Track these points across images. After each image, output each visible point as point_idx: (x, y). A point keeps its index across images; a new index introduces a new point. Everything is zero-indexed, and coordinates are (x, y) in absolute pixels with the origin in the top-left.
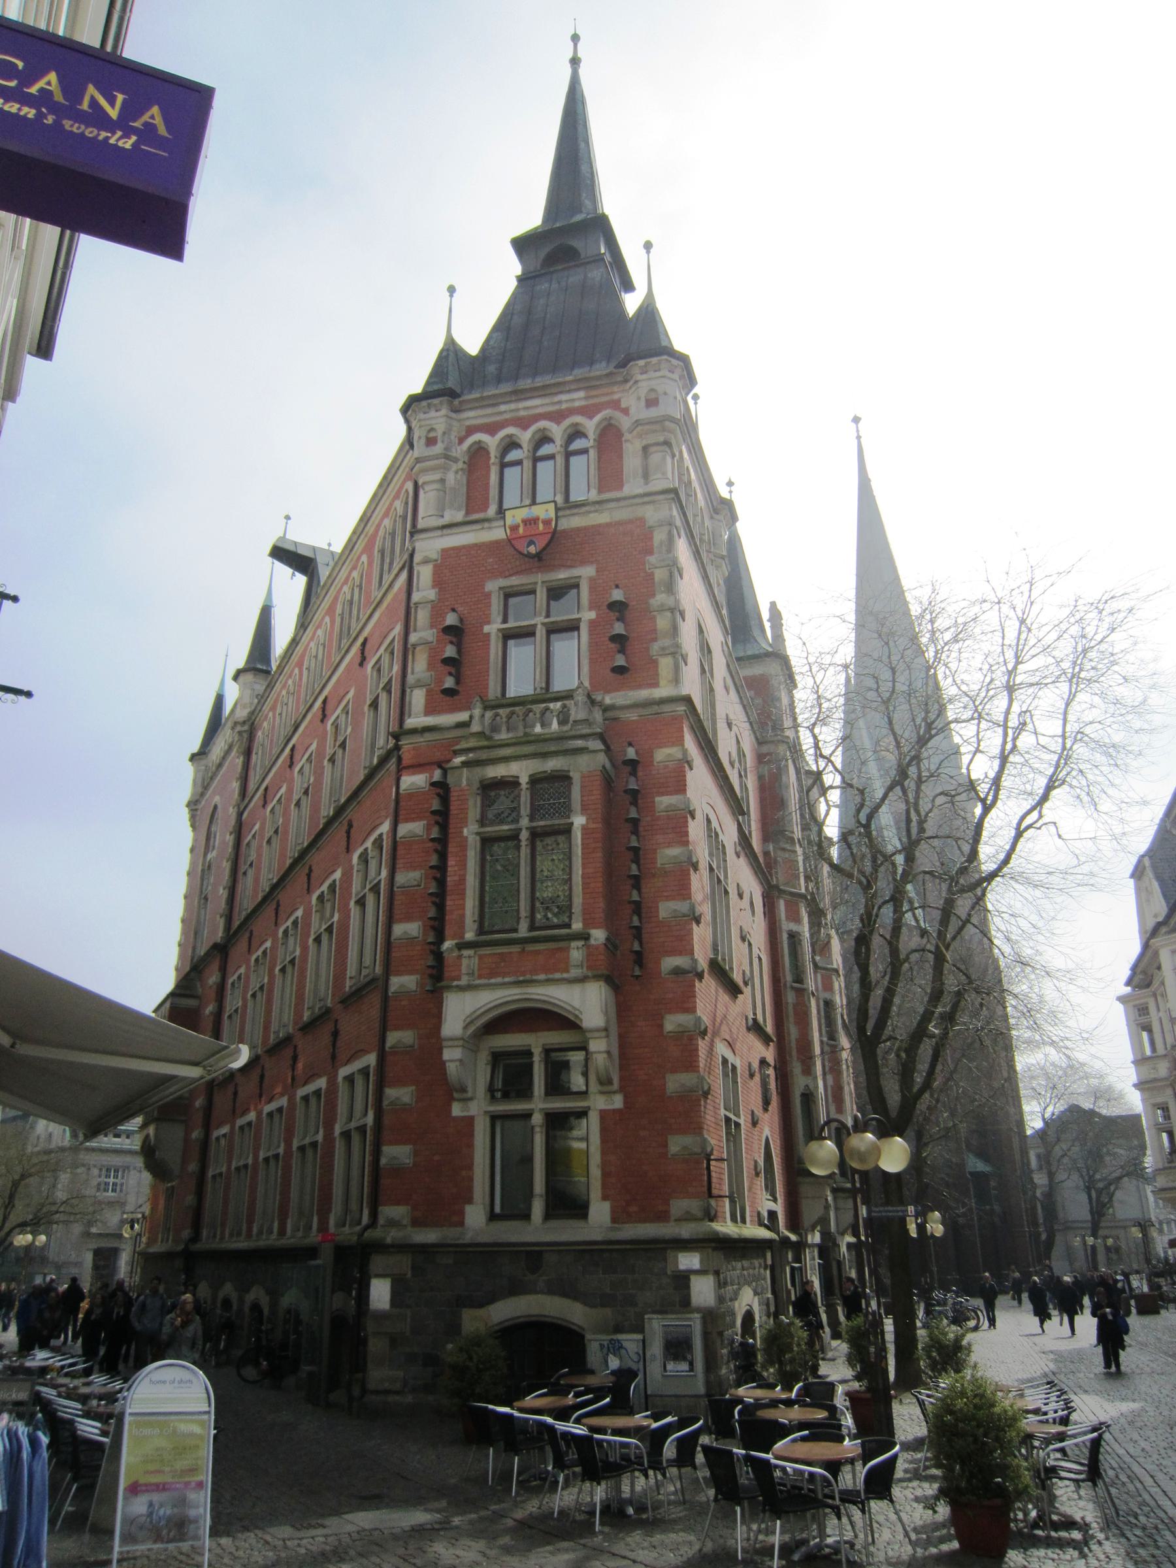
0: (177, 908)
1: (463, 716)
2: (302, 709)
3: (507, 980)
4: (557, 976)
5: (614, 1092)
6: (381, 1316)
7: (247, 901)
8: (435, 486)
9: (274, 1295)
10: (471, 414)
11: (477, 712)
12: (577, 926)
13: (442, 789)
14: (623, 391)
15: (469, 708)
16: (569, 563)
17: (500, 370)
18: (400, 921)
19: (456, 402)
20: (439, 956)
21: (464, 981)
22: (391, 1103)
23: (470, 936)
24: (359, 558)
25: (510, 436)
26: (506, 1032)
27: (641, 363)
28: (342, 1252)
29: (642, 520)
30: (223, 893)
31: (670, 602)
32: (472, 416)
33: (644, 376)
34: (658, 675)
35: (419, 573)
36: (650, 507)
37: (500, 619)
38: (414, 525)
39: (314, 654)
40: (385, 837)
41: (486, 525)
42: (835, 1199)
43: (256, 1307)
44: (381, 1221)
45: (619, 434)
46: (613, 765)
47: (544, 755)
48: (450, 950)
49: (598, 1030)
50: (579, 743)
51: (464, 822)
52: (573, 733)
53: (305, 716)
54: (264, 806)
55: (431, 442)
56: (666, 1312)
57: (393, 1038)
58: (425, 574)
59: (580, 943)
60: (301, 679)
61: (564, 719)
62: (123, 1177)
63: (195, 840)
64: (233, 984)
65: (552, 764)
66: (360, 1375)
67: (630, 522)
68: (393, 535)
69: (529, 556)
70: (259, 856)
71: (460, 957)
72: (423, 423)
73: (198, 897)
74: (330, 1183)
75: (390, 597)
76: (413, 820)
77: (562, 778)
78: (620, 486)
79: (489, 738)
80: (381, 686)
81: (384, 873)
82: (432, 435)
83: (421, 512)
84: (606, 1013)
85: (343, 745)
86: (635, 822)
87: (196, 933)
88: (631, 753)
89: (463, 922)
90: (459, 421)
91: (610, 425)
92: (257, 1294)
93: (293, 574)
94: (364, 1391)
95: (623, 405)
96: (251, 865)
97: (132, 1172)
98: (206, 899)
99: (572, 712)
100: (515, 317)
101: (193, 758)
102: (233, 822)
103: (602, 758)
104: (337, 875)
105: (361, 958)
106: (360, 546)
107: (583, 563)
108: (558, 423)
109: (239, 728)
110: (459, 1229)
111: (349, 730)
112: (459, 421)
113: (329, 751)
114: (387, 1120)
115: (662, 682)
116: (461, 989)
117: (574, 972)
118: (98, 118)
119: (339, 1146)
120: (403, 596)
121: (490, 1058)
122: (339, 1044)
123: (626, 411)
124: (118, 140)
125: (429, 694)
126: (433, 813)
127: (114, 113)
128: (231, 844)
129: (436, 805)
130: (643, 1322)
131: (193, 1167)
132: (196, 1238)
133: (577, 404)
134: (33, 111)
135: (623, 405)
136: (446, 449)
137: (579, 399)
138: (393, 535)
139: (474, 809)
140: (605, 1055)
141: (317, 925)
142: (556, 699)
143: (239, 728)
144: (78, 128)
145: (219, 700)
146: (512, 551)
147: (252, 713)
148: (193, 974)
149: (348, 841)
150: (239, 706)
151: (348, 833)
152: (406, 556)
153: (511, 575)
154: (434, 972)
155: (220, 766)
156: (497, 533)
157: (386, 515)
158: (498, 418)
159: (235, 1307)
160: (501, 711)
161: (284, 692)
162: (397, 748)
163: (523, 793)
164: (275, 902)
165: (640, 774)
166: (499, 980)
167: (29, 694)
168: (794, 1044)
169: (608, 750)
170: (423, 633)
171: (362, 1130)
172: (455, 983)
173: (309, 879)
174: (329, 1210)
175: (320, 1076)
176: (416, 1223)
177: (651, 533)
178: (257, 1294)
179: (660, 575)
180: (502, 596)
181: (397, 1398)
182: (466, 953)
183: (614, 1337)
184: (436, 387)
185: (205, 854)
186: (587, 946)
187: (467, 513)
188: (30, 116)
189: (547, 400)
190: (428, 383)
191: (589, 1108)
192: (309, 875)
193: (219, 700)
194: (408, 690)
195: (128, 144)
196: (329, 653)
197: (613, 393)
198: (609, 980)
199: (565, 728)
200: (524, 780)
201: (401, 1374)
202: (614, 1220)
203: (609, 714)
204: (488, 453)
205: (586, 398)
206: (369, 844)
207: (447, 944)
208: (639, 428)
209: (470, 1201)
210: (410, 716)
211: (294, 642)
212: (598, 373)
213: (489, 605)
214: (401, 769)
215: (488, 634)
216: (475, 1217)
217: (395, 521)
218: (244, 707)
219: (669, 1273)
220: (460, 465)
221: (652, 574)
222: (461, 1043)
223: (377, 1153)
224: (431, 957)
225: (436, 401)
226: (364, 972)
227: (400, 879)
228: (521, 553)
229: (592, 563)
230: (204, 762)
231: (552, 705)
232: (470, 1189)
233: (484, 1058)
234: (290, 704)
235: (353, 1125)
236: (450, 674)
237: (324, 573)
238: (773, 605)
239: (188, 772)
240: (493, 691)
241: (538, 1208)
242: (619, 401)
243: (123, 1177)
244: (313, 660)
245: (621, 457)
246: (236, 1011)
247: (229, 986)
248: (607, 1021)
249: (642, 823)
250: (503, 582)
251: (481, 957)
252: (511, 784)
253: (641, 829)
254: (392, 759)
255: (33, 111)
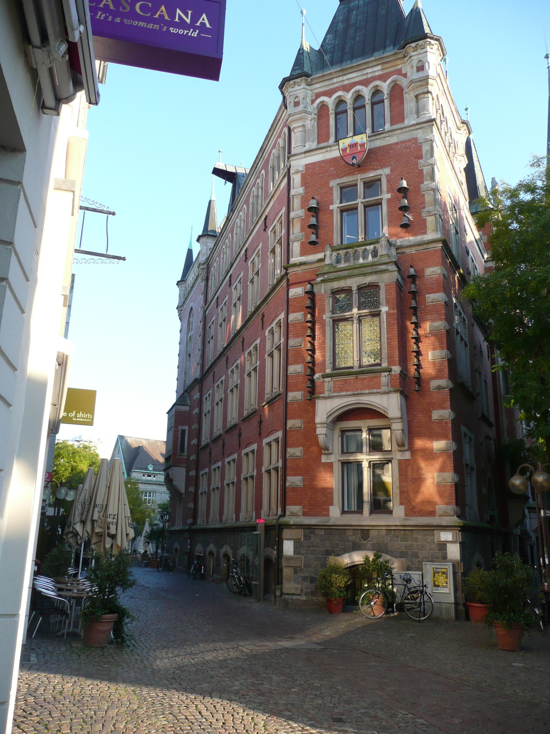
0: (175, 361)
1: (320, 256)
2: (234, 255)
3: (348, 393)
4: (375, 391)
5: (406, 451)
6: (289, 558)
7: (210, 358)
8: (300, 129)
9: (235, 550)
10: (318, 85)
11: (328, 253)
12: (385, 365)
13: (311, 294)
14: (403, 63)
15: (323, 251)
16: (375, 167)
17: (332, 57)
18: (292, 364)
19: (309, 79)
20: (312, 381)
21: (326, 394)
22: (291, 456)
23: (328, 371)
24: (260, 171)
25: (340, 97)
26: (349, 420)
27: (413, 45)
28: (268, 528)
29: (416, 139)
30: (198, 353)
31: (433, 185)
32: (319, 87)
33: (415, 53)
34: (426, 227)
35: (293, 179)
36: (420, 131)
37: (338, 201)
38: (289, 152)
39: (239, 225)
40: (282, 321)
41: (329, 149)
42: (529, 512)
43: (226, 556)
44: (288, 513)
45: (402, 89)
46: (402, 278)
47: (365, 274)
48: (319, 378)
49: (397, 419)
50: (383, 267)
51: (323, 311)
52: (380, 262)
53: (236, 259)
54: (217, 307)
55: (297, 104)
56: (434, 562)
57: (290, 423)
58: (297, 179)
59: (387, 374)
60: (233, 239)
61: (375, 253)
62: (153, 496)
63: (182, 326)
64: (206, 398)
65: (369, 279)
66: (280, 586)
67: (409, 141)
68: (278, 158)
69: (353, 165)
70: (216, 333)
71: (323, 382)
72: (291, 94)
73: (185, 355)
74: (261, 495)
75: (278, 193)
76: (297, 312)
77: (375, 286)
78: (402, 120)
79: (334, 267)
80: (276, 241)
81: (282, 340)
82: (297, 100)
83: (293, 145)
84: (401, 410)
85: (257, 274)
86: (415, 309)
87: (185, 373)
88: (412, 271)
89: (325, 364)
90: (311, 90)
91: (396, 84)
92: (226, 549)
93: (226, 183)
94: (282, 594)
95: (403, 72)
96: (212, 338)
97: (158, 494)
98: (189, 355)
99: (379, 251)
100: (340, 24)
101: (178, 283)
102: (201, 316)
103: (396, 275)
104: (258, 341)
105: (272, 385)
106: (260, 165)
107: (383, 167)
108: (366, 86)
109: (201, 267)
110: (326, 518)
111: (260, 266)
112: (311, 90)
113: (250, 277)
114: (288, 464)
115: (428, 232)
116: (325, 398)
117: (384, 389)
118: (182, 24)
119: (265, 477)
120: (286, 191)
121: (340, 433)
122: (262, 426)
123: (405, 75)
124: (191, 33)
125: (302, 244)
126: (307, 307)
127: (188, 21)
128: (201, 327)
129: (308, 303)
130: (422, 566)
131: (192, 489)
132: (195, 522)
133: (377, 74)
134: (158, 26)
135: (403, 72)
136: (305, 107)
137: (378, 71)
138: (278, 158)
139: (328, 303)
140: (401, 431)
141: (248, 368)
142: (370, 244)
143: (201, 267)
144: (176, 31)
145: (190, 252)
146: (344, 163)
147: (208, 259)
148: (186, 394)
149: (263, 324)
150: (200, 255)
151: (262, 320)
152: (286, 170)
153: (343, 177)
154: (310, 390)
155: (192, 287)
156: (335, 153)
157: (274, 147)
158: (332, 87)
159: (215, 556)
160: (340, 252)
161: (224, 247)
162: (286, 274)
163: (354, 295)
164: (226, 356)
165: (417, 282)
166: (344, 393)
167: (124, 259)
168: (505, 428)
169: (399, 270)
170: (298, 212)
171: (276, 469)
172: (322, 395)
173: (243, 344)
174: (261, 508)
175: (254, 443)
176: (305, 514)
177: (421, 146)
178: (226, 549)
179: (426, 170)
180: (339, 188)
181: (298, 597)
182: (326, 379)
183: (407, 572)
184: (297, 72)
185: (188, 333)
186: (391, 375)
187: (319, 143)
188: (158, 29)
189: (359, 73)
190: (293, 70)
191: (392, 458)
192: (243, 342)
193: (190, 252)
194: (291, 243)
195: (195, 34)
196: (247, 224)
197: (397, 65)
198: (402, 393)
199: (376, 259)
200: (354, 288)
201: (300, 586)
202: (406, 515)
203: (399, 251)
204: (328, 108)
205: (382, 69)
206: (274, 325)
207: (316, 376)
208: (413, 85)
209: (332, 504)
210: (292, 257)
211: (228, 219)
212: (388, 54)
213: (332, 194)
214: (289, 286)
215: (332, 210)
216: (335, 512)
217: (279, 150)
218: (203, 255)
219: (436, 542)
220: (313, 116)
221: (422, 170)
222: (325, 425)
223: (284, 480)
224: (309, 382)
225: (298, 80)
226: (274, 391)
227: (291, 342)
228: (348, 164)
229: (388, 166)
230: (184, 285)
231: (368, 247)
232: (332, 499)
233: (337, 433)
234: (228, 253)
235: (272, 467)
236: (313, 233)
237: (242, 181)
238: (493, 179)
239: (176, 291)
240: (336, 241)
241: (366, 508)
242: (400, 70)
243: (153, 496)
244: (239, 229)
245: (402, 103)
246: (209, 412)
247: (204, 400)
248: (402, 414)
249: (419, 310)
250: (339, 181)
251: (335, 382)
252: (348, 291)
253: (418, 312)
254: (286, 280)
255: (158, 26)
